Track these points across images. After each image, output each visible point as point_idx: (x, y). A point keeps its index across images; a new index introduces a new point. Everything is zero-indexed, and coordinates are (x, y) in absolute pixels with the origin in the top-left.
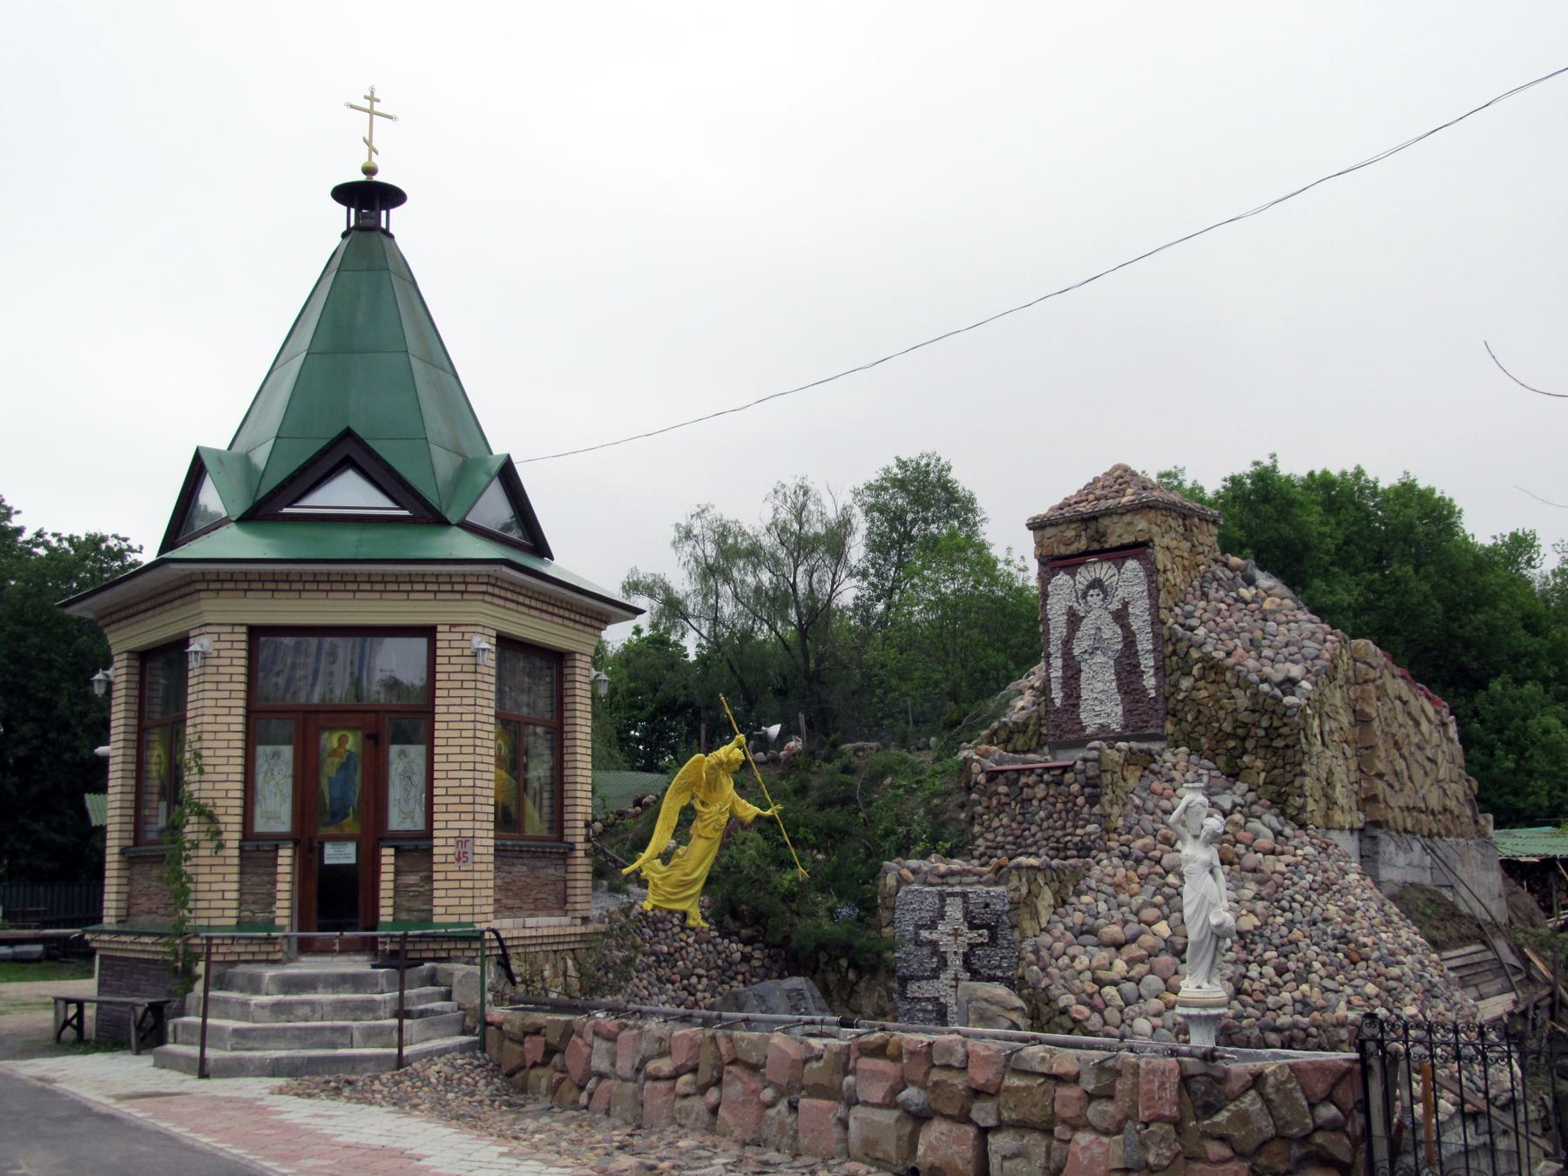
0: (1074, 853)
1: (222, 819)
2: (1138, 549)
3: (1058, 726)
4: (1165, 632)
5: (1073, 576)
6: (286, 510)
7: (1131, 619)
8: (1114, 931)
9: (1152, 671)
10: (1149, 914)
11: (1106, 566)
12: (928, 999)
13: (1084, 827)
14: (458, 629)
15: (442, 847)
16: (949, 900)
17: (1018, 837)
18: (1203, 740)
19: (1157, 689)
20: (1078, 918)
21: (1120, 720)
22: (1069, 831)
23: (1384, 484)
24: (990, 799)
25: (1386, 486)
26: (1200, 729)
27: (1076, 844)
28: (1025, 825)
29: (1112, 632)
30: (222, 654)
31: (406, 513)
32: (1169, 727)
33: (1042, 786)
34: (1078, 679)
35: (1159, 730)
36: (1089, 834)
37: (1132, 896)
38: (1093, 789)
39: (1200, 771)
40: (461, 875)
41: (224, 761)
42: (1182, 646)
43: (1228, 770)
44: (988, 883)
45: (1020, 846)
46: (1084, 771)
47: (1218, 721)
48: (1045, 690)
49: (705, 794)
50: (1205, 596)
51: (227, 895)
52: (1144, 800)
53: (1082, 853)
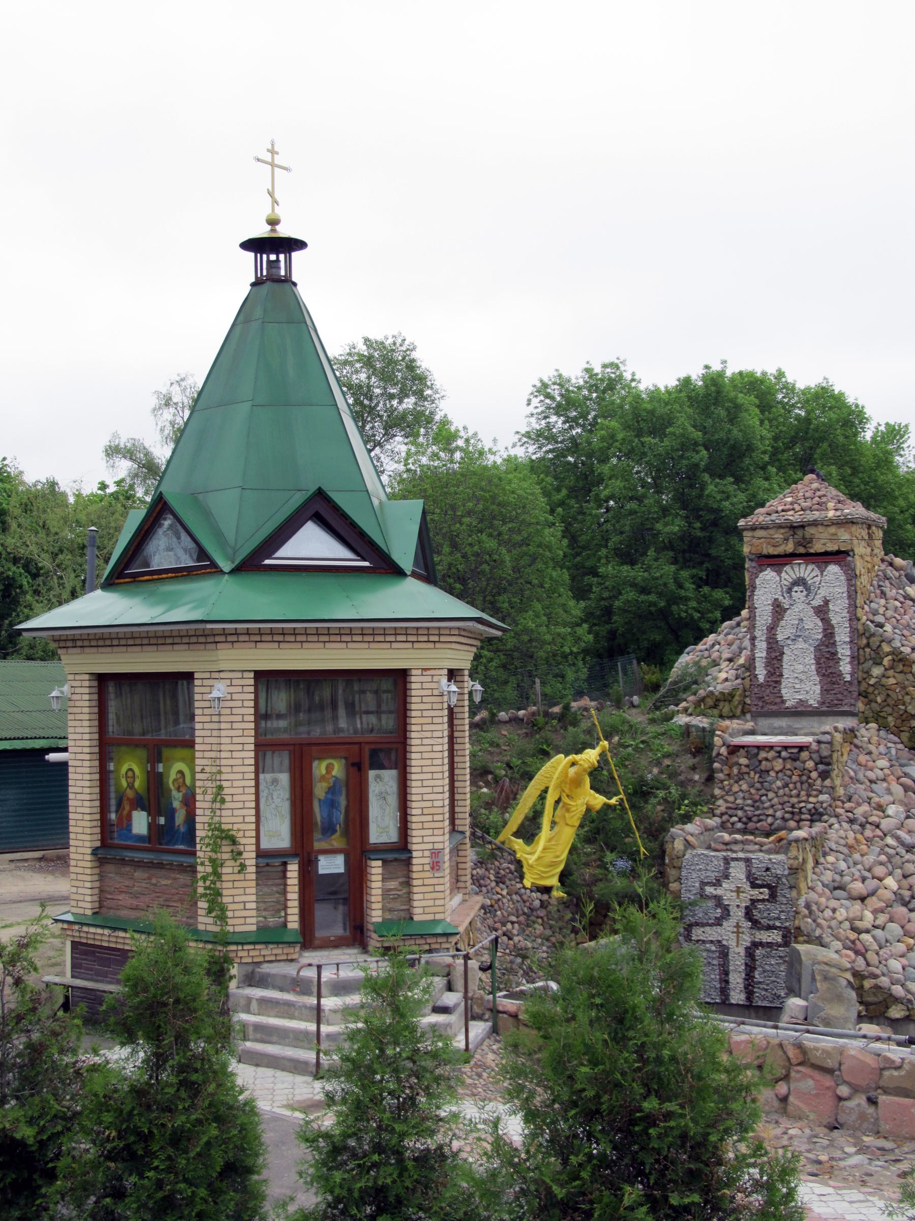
0: (808, 817)
1: (242, 841)
2: (840, 556)
3: (761, 698)
4: (860, 627)
5: (779, 573)
6: (267, 562)
7: (831, 615)
8: (858, 887)
9: (848, 659)
10: (880, 871)
11: (810, 567)
12: (712, 942)
13: (817, 796)
14: (428, 673)
15: (420, 859)
16: (732, 864)
17: (755, 801)
18: (890, 719)
19: (852, 675)
20: (828, 876)
21: (818, 697)
22: (804, 798)
23: (801, 385)
24: (731, 767)
25: (802, 388)
26: (888, 710)
27: (810, 810)
28: (763, 792)
29: (814, 625)
30: (235, 697)
31: (366, 564)
32: (860, 706)
33: (780, 761)
34: (781, 660)
35: (852, 709)
36: (822, 803)
37: (862, 855)
38: (825, 764)
39: (890, 745)
40: (435, 881)
41: (240, 791)
42: (875, 641)
43: (909, 744)
44: (769, 852)
45: (758, 808)
46: (818, 751)
47: (904, 704)
48: (750, 666)
49: (570, 790)
50: (883, 594)
51: (248, 906)
52: (855, 772)
53: (815, 817)
